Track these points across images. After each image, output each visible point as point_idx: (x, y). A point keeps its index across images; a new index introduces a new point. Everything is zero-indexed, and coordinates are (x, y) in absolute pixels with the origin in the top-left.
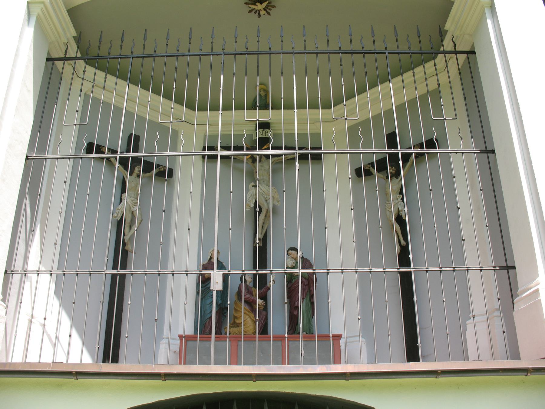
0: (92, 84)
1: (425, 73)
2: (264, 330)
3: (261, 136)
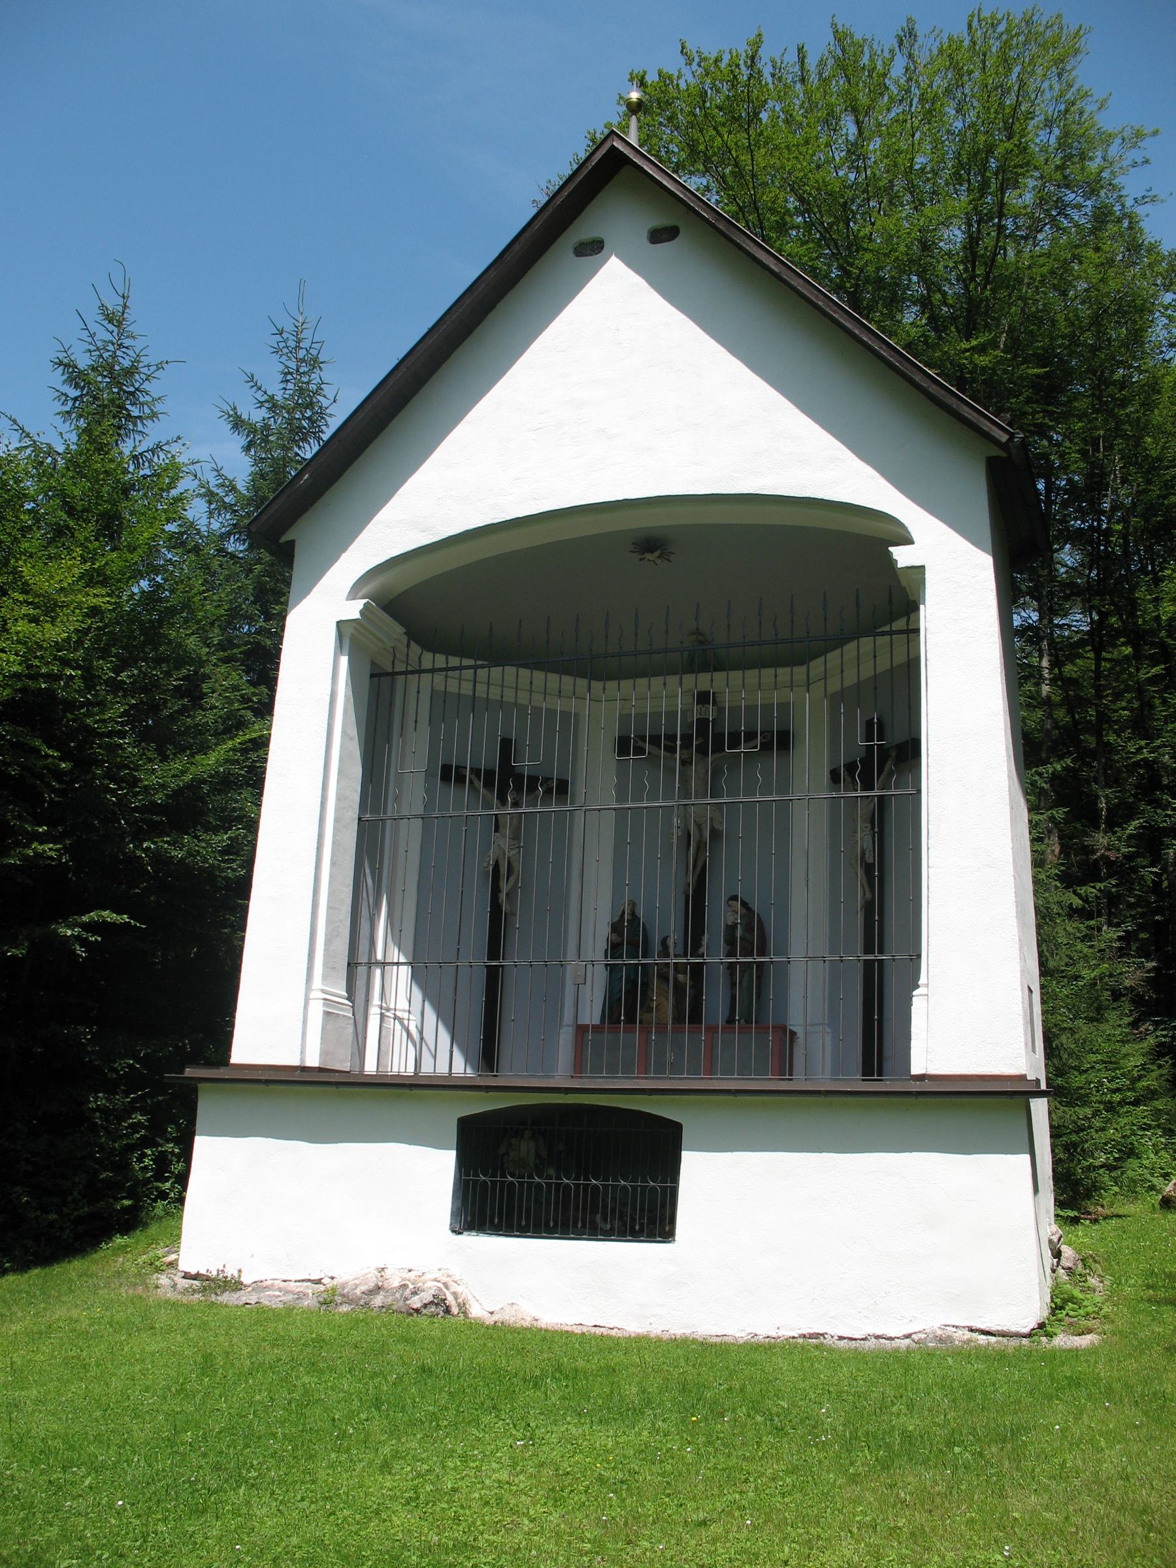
0: (478, 670)
1: (808, 675)
2: (696, 1018)
3: (699, 716)
